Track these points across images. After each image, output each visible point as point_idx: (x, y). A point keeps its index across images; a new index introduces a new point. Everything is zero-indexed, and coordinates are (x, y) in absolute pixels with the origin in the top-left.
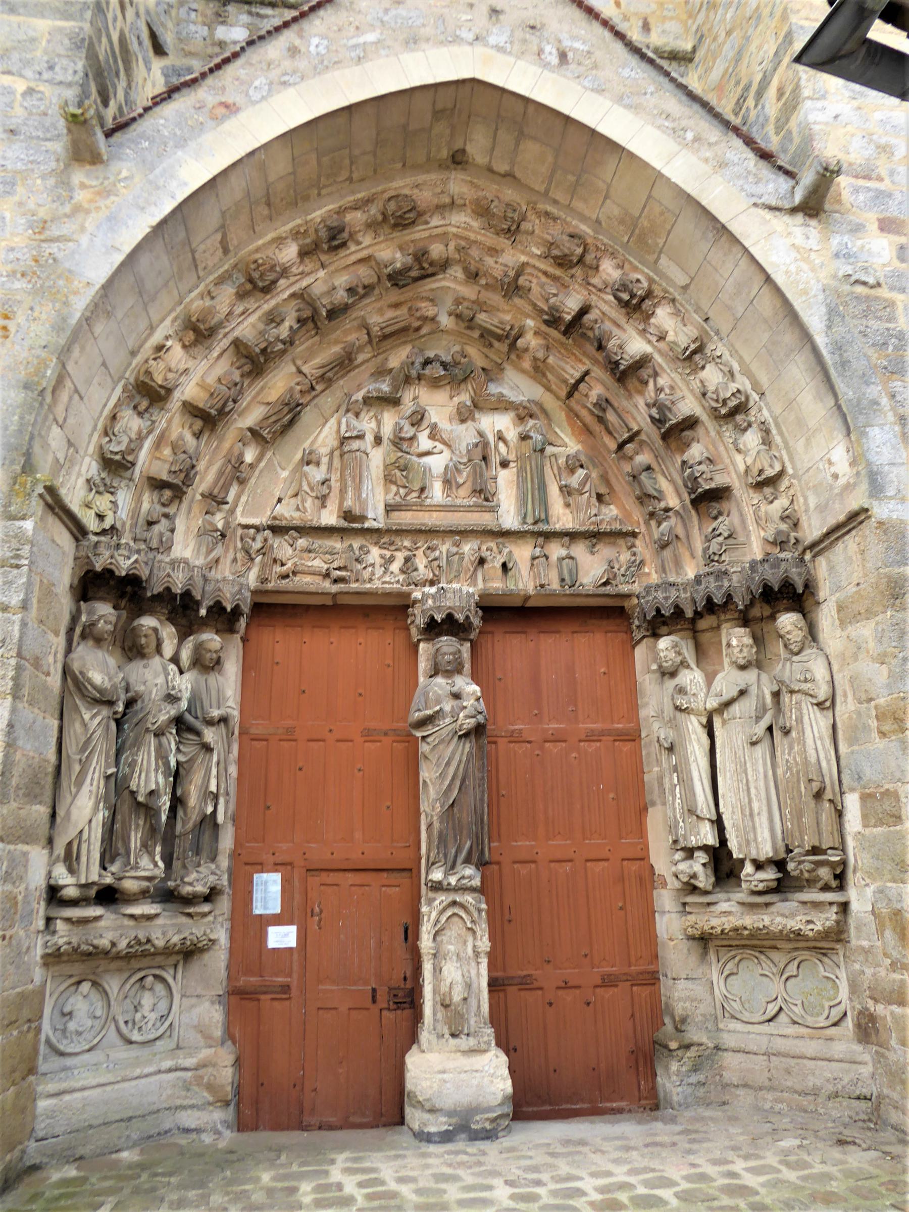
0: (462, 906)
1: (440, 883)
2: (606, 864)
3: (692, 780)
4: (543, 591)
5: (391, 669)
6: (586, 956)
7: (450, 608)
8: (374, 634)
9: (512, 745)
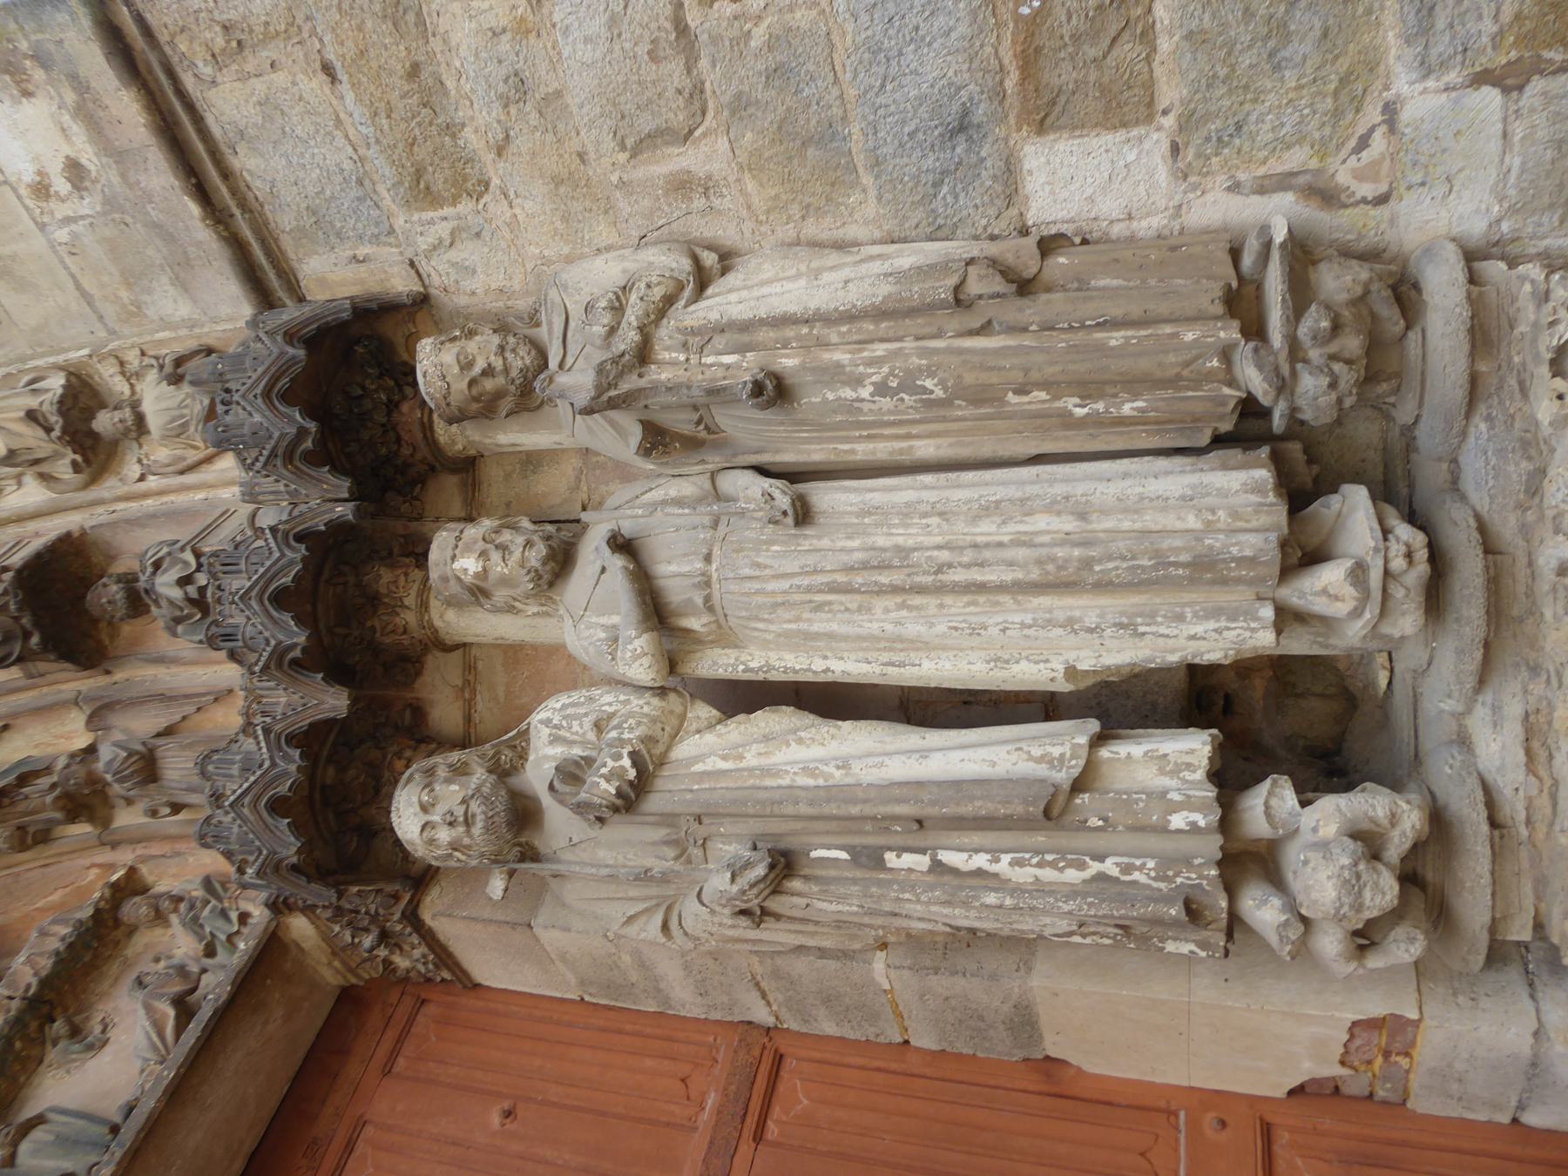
3: (920, 784)
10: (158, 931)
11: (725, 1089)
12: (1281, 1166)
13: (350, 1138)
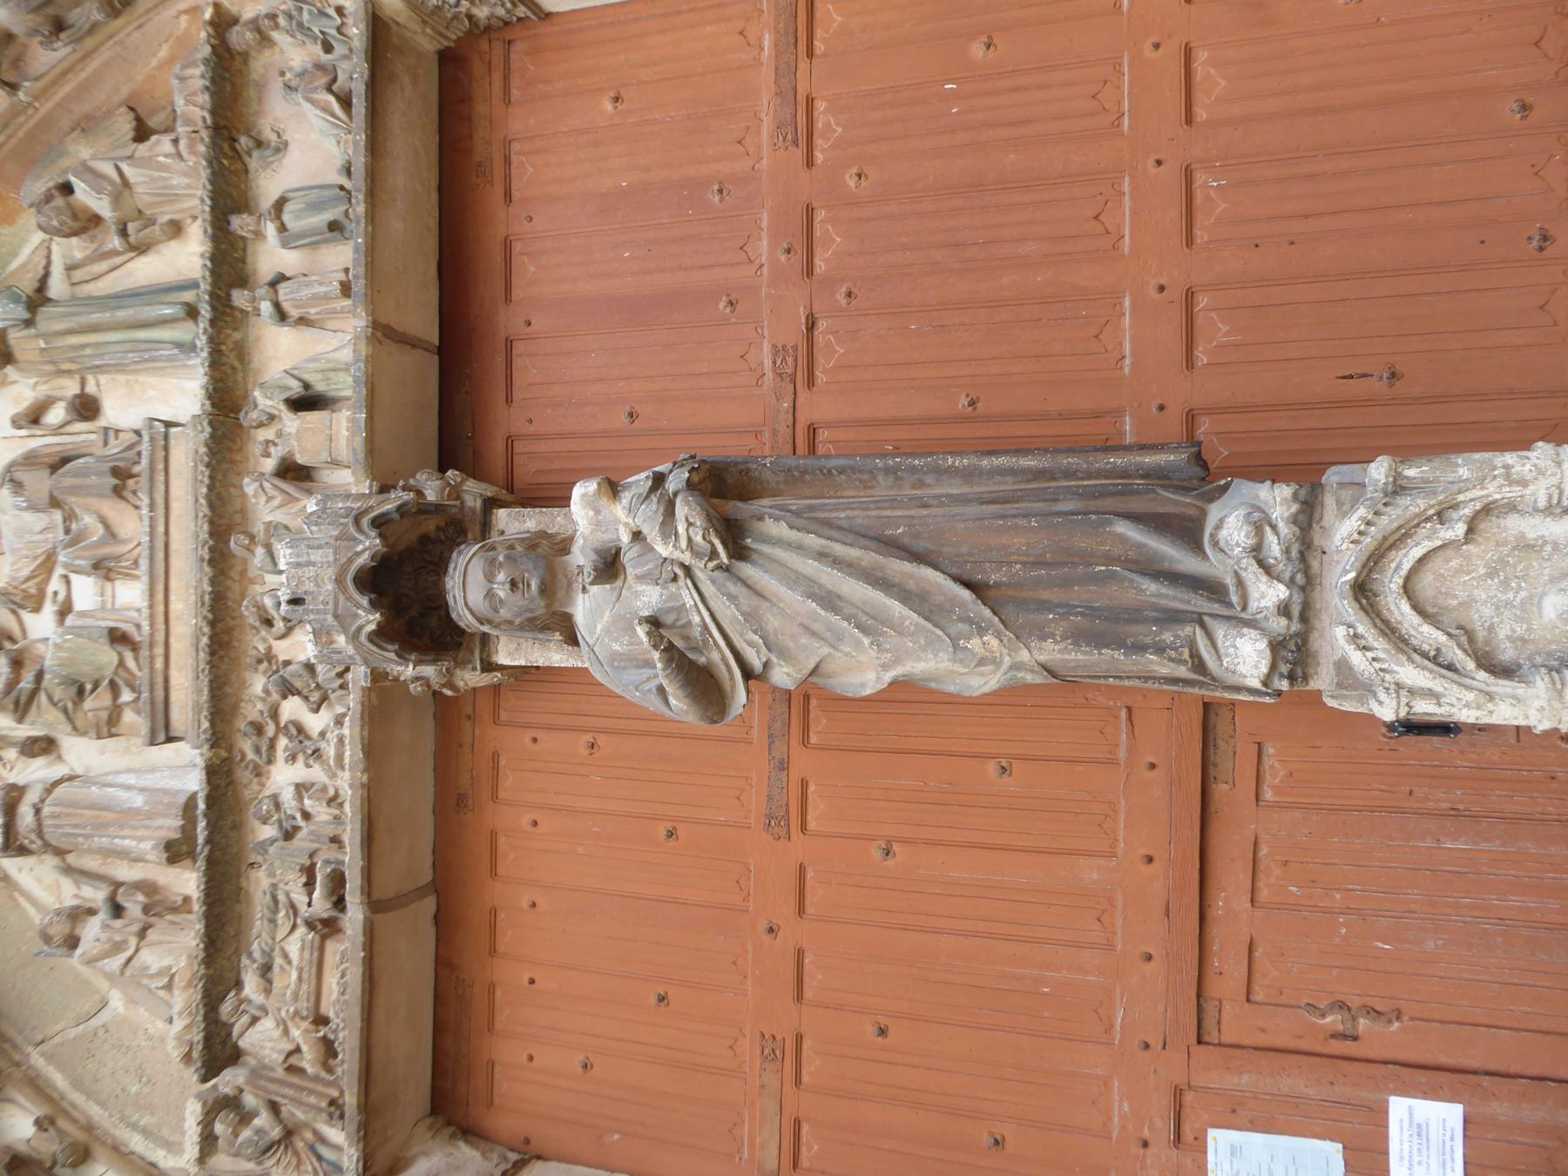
0: (1375, 560)
1: (1276, 646)
2: (1201, 56)
4: (359, 286)
5: (602, 740)
6: (1525, 108)
7: (339, 580)
8: (508, 781)
9: (820, 377)
10: (267, 53)
11: (775, 28)
12: (1562, 1073)
13: (505, 155)
